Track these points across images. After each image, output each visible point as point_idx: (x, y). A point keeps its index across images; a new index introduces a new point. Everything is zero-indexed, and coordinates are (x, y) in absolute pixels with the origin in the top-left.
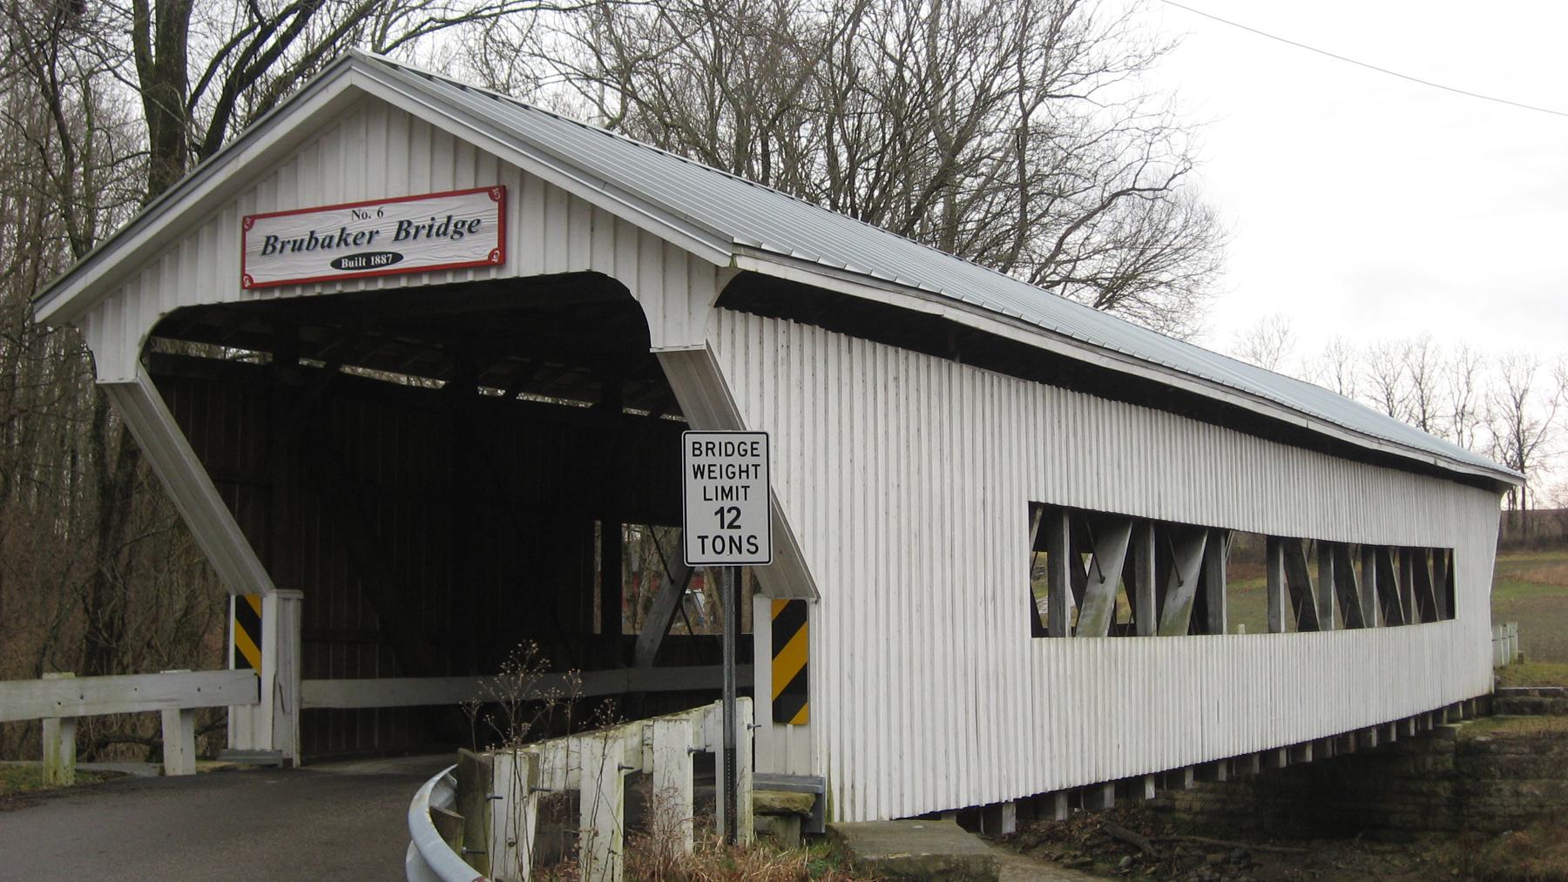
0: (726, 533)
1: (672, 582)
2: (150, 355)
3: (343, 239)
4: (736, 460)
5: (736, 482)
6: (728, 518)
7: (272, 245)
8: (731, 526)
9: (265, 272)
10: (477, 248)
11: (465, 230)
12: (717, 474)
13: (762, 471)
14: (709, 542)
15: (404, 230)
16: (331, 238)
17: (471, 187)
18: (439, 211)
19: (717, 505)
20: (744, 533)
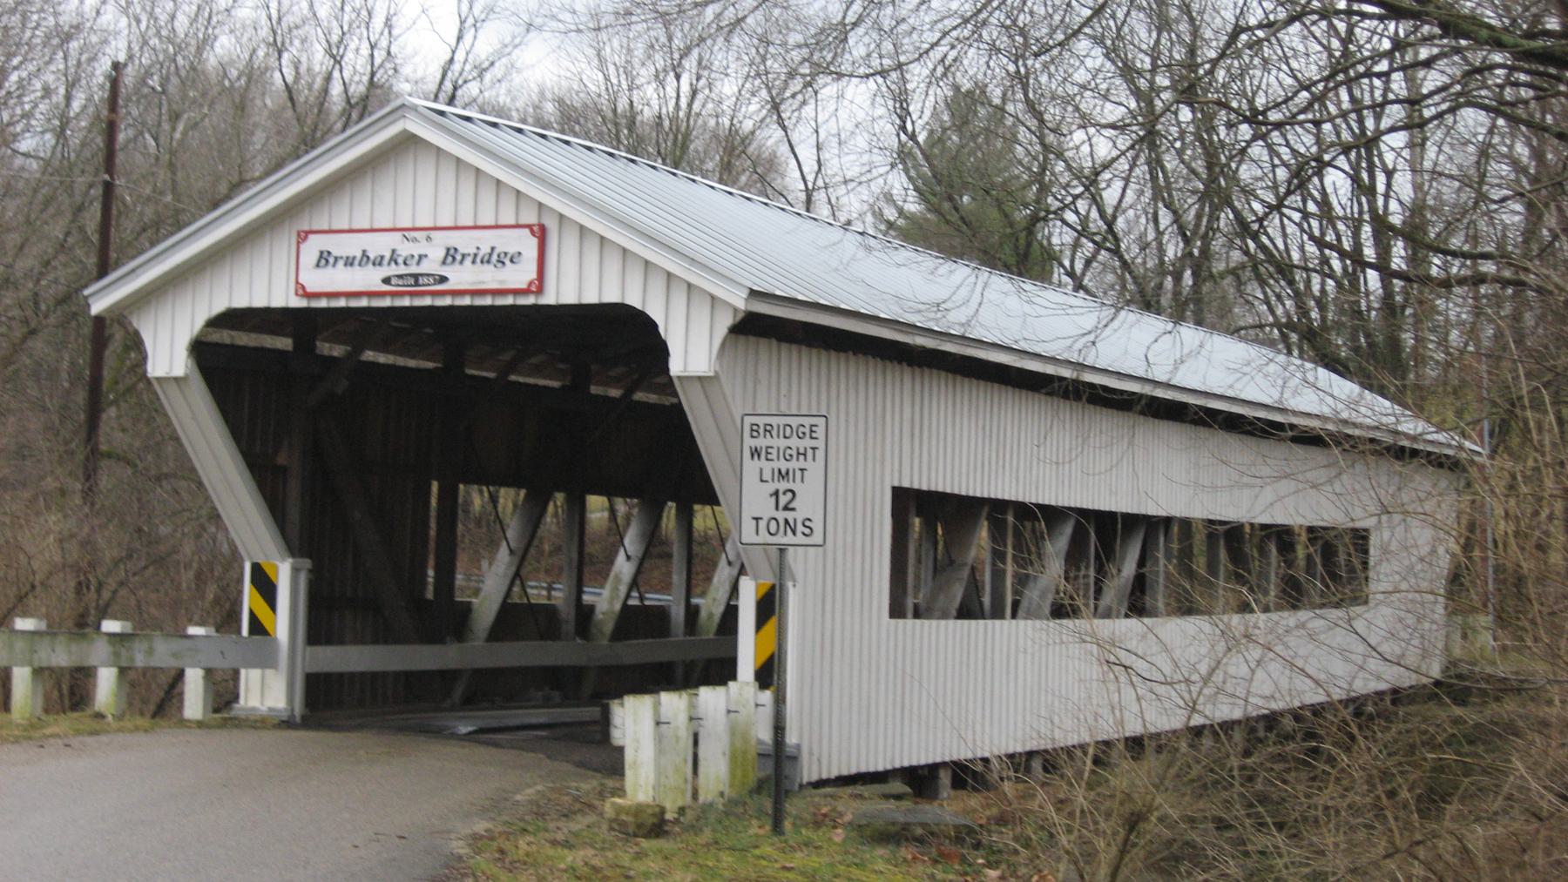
0: (781, 515)
1: (512, 552)
2: (200, 349)
3: (393, 260)
4: (794, 442)
5: (794, 465)
6: (783, 500)
7: (324, 259)
8: (786, 508)
9: (317, 280)
10: (520, 275)
11: (507, 261)
12: (774, 456)
13: (820, 454)
14: (762, 524)
15: (451, 255)
16: (382, 257)
17: (513, 222)
18: (485, 241)
19: (771, 487)
20: (799, 515)
